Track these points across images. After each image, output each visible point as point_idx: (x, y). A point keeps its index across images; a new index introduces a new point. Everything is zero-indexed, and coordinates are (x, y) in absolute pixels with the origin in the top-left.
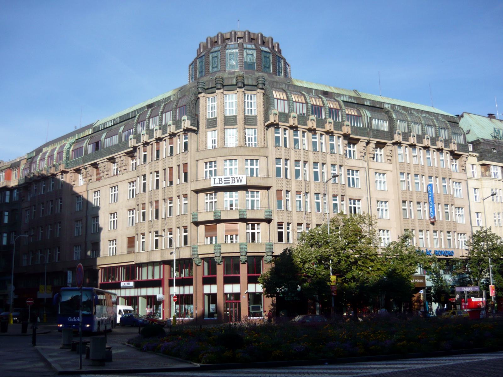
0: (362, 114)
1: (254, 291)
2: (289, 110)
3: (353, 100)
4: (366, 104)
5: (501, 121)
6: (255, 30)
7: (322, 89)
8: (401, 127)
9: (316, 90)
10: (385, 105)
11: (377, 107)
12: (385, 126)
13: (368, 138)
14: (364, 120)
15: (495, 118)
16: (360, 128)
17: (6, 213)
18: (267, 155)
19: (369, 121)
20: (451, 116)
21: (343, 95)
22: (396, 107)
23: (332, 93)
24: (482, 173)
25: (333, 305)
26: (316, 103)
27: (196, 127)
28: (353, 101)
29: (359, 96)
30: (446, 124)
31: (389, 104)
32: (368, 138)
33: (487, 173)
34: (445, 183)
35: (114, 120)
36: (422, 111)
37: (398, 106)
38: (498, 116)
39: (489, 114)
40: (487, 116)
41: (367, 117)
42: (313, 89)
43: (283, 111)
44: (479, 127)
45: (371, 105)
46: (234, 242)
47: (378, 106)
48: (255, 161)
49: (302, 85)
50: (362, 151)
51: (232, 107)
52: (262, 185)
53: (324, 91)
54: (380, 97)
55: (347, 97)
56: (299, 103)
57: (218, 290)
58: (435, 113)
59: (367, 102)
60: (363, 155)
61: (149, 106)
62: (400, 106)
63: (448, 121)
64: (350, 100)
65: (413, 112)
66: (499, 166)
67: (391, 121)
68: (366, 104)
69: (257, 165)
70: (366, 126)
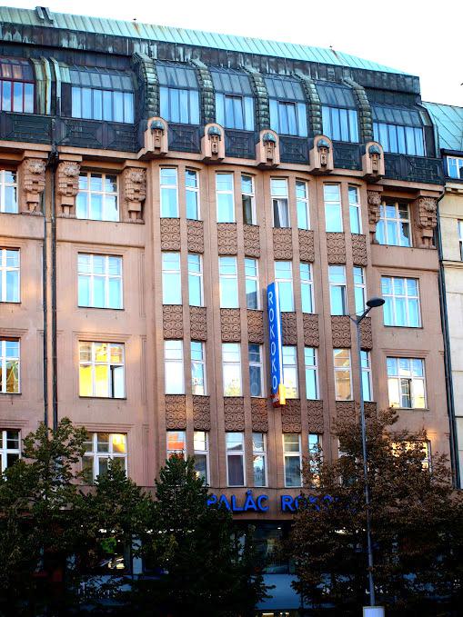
0: (39, 76)
2: (257, 123)
4: (65, 44)
8: (179, 107)
10: (137, 47)
11: (107, 54)
12: (123, 111)
13: (48, 148)
14: (40, 92)
16: (22, 117)
19: (59, 95)
22: (181, 50)
25: (371, 564)
29: (46, 24)
30: (356, 97)
32: (48, 148)
34: (258, 360)
41: (54, 83)
43: (293, 132)
50: (132, 197)
56: (102, 89)
59: (69, 39)
60: (137, 207)
63: (366, 88)
65: (241, 64)
67: (143, 97)
70: (48, 112)
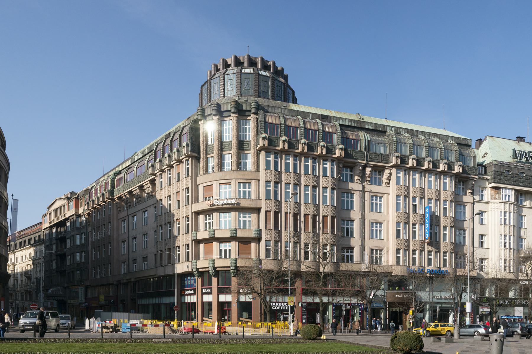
1: (244, 300)
3: (353, 123)
5: (530, 144)
6: (258, 56)
7: (320, 113)
9: (313, 114)
10: (388, 128)
15: (524, 141)
17: (394, 296)
18: (258, 178)
19: (367, 144)
20: (463, 138)
21: (343, 119)
22: (401, 130)
23: (331, 117)
24: (492, 196)
26: (329, 129)
27: (196, 153)
28: (353, 124)
31: (393, 127)
33: (497, 196)
35: (144, 151)
36: (430, 133)
37: (403, 128)
38: (527, 139)
39: (517, 138)
40: (516, 139)
42: (310, 113)
44: (494, 151)
45: (373, 128)
46: (228, 257)
47: (380, 129)
48: (247, 184)
49: (299, 110)
51: (229, 133)
52: (252, 206)
53: (322, 115)
54: (385, 120)
55: (347, 120)
57: (213, 299)
58: (444, 135)
61: (167, 136)
62: (405, 129)
64: (350, 124)
66: (512, 189)
68: (367, 127)
69: (249, 188)
